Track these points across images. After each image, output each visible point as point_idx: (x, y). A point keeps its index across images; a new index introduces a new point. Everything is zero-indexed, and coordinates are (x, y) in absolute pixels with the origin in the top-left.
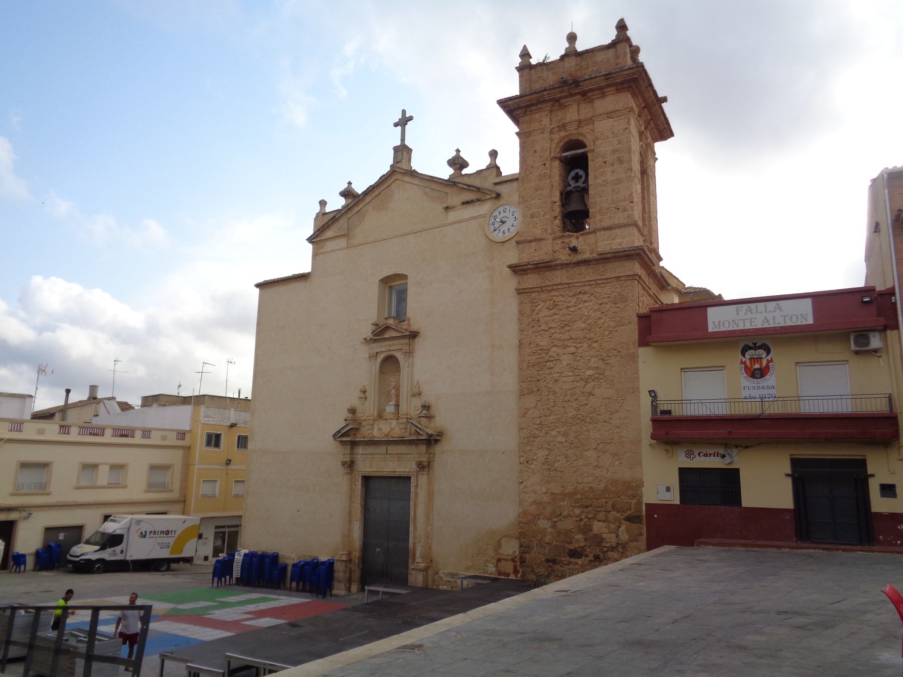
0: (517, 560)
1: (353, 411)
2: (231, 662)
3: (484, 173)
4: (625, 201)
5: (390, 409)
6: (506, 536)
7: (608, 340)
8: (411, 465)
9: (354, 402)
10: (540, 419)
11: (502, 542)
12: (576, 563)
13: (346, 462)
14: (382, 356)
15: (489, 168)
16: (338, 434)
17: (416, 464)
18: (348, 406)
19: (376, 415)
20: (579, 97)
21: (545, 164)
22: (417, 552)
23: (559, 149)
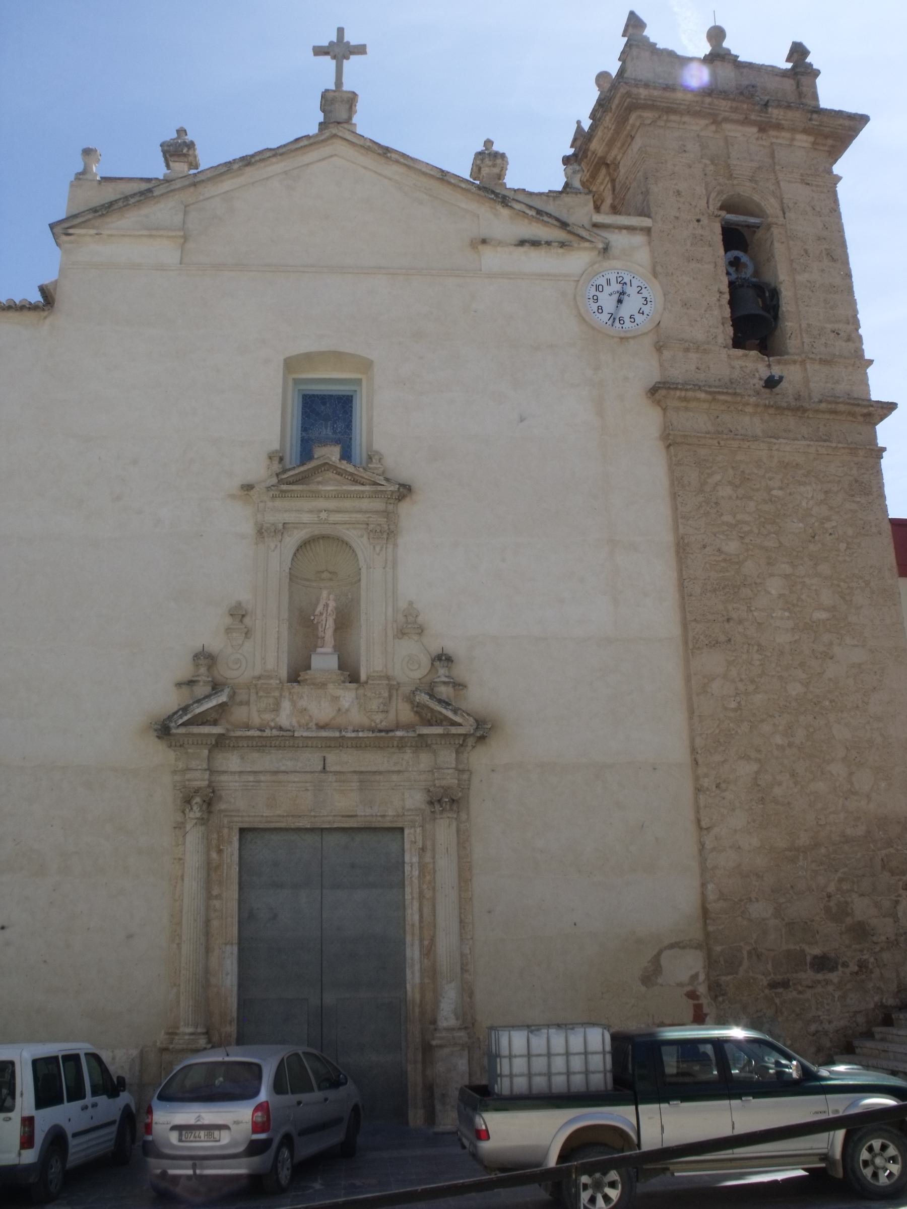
0: (702, 990)
4: (848, 323)
6: (672, 946)
7: (848, 559)
8: (403, 800)
10: (738, 699)
11: (664, 960)
12: (827, 982)
13: (197, 791)
14: (300, 535)
18: (196, 644)
19: (284, 673)
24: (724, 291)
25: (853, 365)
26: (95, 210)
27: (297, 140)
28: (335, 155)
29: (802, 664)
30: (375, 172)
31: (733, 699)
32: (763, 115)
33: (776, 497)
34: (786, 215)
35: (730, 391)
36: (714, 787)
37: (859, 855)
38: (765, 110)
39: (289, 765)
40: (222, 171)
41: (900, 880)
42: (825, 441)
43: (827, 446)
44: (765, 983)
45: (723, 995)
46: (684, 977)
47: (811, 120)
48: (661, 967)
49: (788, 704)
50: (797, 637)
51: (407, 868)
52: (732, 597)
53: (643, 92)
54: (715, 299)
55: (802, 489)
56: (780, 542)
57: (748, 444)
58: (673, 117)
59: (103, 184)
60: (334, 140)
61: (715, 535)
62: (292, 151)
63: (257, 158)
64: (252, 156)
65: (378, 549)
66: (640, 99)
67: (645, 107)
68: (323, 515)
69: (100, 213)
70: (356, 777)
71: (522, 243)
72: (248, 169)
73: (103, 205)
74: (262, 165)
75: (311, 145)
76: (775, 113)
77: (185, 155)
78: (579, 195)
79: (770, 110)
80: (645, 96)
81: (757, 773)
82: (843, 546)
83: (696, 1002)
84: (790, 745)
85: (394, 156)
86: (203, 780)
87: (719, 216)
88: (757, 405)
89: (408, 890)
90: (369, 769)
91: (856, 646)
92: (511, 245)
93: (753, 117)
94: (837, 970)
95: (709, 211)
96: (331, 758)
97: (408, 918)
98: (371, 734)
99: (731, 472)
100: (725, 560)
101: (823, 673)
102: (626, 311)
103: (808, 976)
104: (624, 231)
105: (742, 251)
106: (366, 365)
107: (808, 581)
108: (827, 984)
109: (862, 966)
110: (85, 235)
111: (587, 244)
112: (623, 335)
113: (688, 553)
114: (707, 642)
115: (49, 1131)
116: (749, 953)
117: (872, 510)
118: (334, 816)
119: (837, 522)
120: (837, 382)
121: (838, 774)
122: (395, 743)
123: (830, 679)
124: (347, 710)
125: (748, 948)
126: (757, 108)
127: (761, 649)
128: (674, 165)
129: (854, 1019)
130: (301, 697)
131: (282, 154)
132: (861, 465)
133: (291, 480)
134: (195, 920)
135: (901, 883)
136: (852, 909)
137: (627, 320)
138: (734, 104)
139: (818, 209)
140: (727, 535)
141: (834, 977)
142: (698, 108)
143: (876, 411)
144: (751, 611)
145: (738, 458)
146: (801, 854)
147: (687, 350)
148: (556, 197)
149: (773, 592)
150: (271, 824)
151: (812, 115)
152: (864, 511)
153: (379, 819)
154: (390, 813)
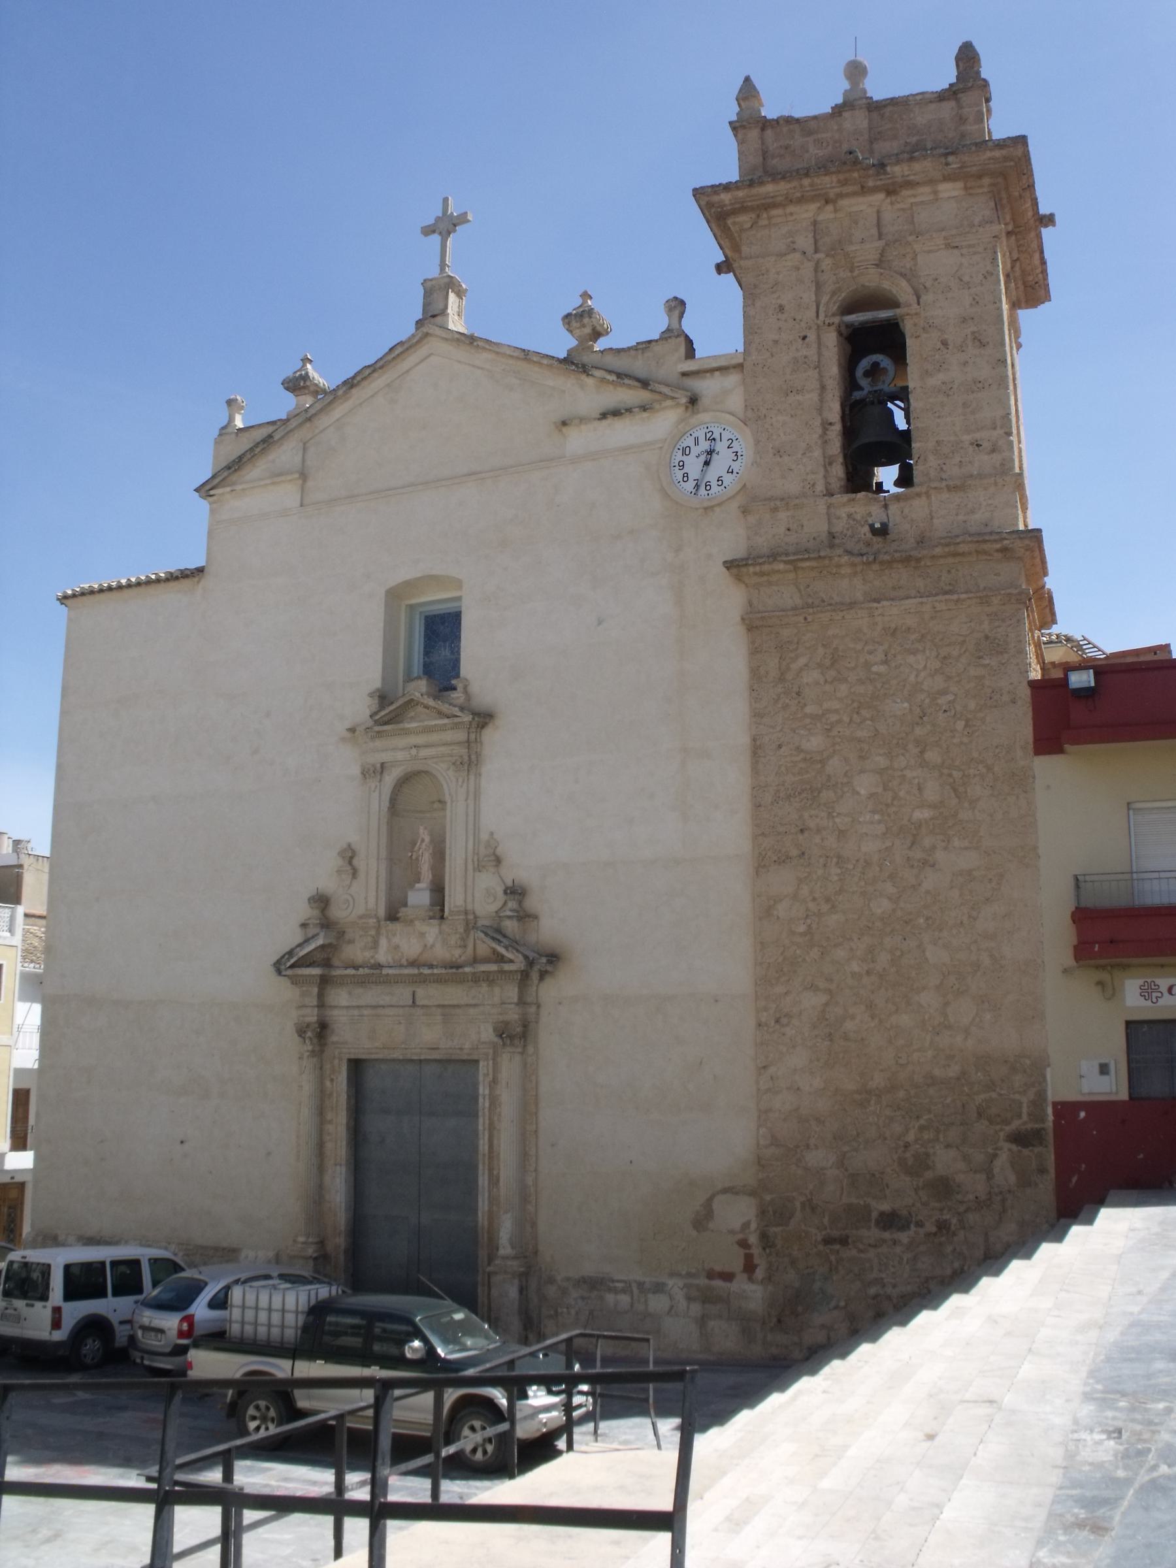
0: (753, 1239)
1: (322, 901)
2: (682, 370)
3: (656, 348)
4: (995, 428)
5: (420, 897)
6: (725, 1191)
7: (965, 740)
8: (479, 1033)
9: (326, 882)
10: (809, 921)
12: (895, 1242)
13: (308, 1025)
15: (667, 334)
16: (288, 960)
17: (495, 1030)
19: (382, 912)
20: (881, 196)
21: (804, 338)
22: (501, 1234)
23: (835, 308)
24: (833, 421)
25: (996, 484)
26: (228, 467)
27: (391, 349)
28: (431, 354)
29: (892, 877)
30: (469, 364)
32: (882, 177)
33: (877, 673)
34: (921, 300)
35: (812, 556)
36: (773, 1023)
37: (949, 1100)
38: (882, 171)
39: (387, 1000)
40: (329, 400)
41: (1001, 1130)
42: (946, 593)
43: (946, 600)
44: (819, 1238)
45: (770, 1247)
46: (737, 1224)
47: (947, 164)
48: (712, 1212)
49: (870, 925)
50: (888, 844)
51: (481, 1100)
52: (810, 802)
53: (725, 197)
54: (816, 436)
55: (911, 659)
56: (876, 730)
57: (841, 614)
58: (774, 212)
59: (240, 435)
61: (795, 732)
62: (390, 362)
63: (358, 378)
64: (353, 378)
65: (460, 780)
66: (725, 205)
67: (734, 212)
68: (414, 752)
69: (233, 469)
70: (439, 1011)
71: (604, 416)
72: (354, 391)
73: (234, 461)
75: (407, 349)
76: (897, 171)
77: (304, 387)
78: (669, 341)
79: (888, 169)
80: (730, 200)
81: (827, 1004)
82: (960, 725)
83: (747, 1251)
84: (868, 973)
85: (480, 344)
86: (313, 1016)
87: (833, 323)
88: (853, 565)
89: (481, 1120)
90: (451, 1003)
91: (966, 848)
92: (595, 419)
93: (871, 183)
94: (908, 1228)
95: (819, 322)
96: (420, 992)
97: (481, 1148)
98: (443, 971)
99: (821, 651)
100: (805, 760)
101: (920, 885)
102: (712, 475)
103: (873, 1233)
104: (717, 373)
105: (880, 353)
107: (909, 774)
108: (895, 1244)
109: (942, 1226)
110: (223, 494)
111: (669, 403)
112: (706, 504)
114: (775, 858)
115: (83, 1318)
116: (803, 1204)
117: (1005, 673)
118: (421, 1048)
119: (956, 695)
120: (973, 512)
121: (929, 1005)
122: (470, 978)
123: (928, 892)
124: (432, 946)
125: (803, 1199)
126: (871, 172)
127: (840, 860)
128: (778, 273)
129: (925, 1285)
130: (394, 935)
131: (381, 367)
132: (996, 615)
133: (386, 719)
134: (307, 1143)
135: (1002, 1134)
136: (933, 1162)
137: (714, 483)
138: (841, 177)
139: (966, 278)
140: (809, 730)
141: (904, 1237)
142: (798, 195)
143: (1013, 543)
144: (833, 817)
145: (830, 633)
146: (874, 1098)
147: (775, 510)
148: (646, 348)
149: (863, 792)
151: (946, 158)
152: (994, 675)
153: (458, 1051)
154: (467, 1046)
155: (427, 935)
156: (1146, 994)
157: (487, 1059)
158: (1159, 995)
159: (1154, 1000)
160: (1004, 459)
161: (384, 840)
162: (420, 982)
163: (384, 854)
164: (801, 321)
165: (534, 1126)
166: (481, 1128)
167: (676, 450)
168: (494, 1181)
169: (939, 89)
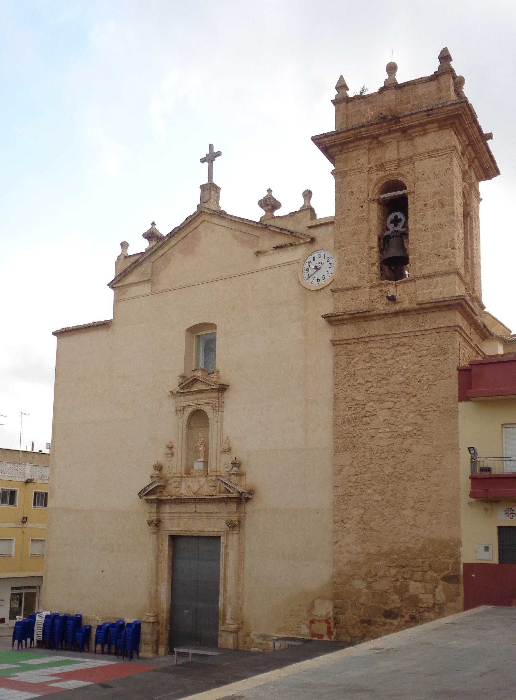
1: (159, 468)
3: (298, 215)
4: (447, 247)
5: (198, 466)
6: (319, 597)
7: (428, 394)
10: (356, 477)
12: (392, 624)
13: (152, 521)
16: (144, 492)
17: (226, 523)
19: (183, 472)
21: (362, 207)
27: (187, 219)
31: (354, 477)
44: (358, 620)
60: (202, 213)
63: (173, 233)
65: (215, 414)
74: (177, 235)
84: (382, 500)
96: (198, 506)
97: (221, 575)
104: (324, 226)
106: (213, 326)
113: (337, 403)
124: (203, 486)
137: (321, 278)
150: (191, 532)
151: (428, 112)
155: (201, 482)
156: (508, 514)
157: (224, 536)
158: (514, 515)
159: (511, 517)
160: (450, 262)
161: (184, 440)
162: (198, 502)
163: (184, 446)
164: (360, 199)
165: (243, 566)
166: (221, 566)
167: (305, 263)
168: (225, 590)
169: (429, 75)
